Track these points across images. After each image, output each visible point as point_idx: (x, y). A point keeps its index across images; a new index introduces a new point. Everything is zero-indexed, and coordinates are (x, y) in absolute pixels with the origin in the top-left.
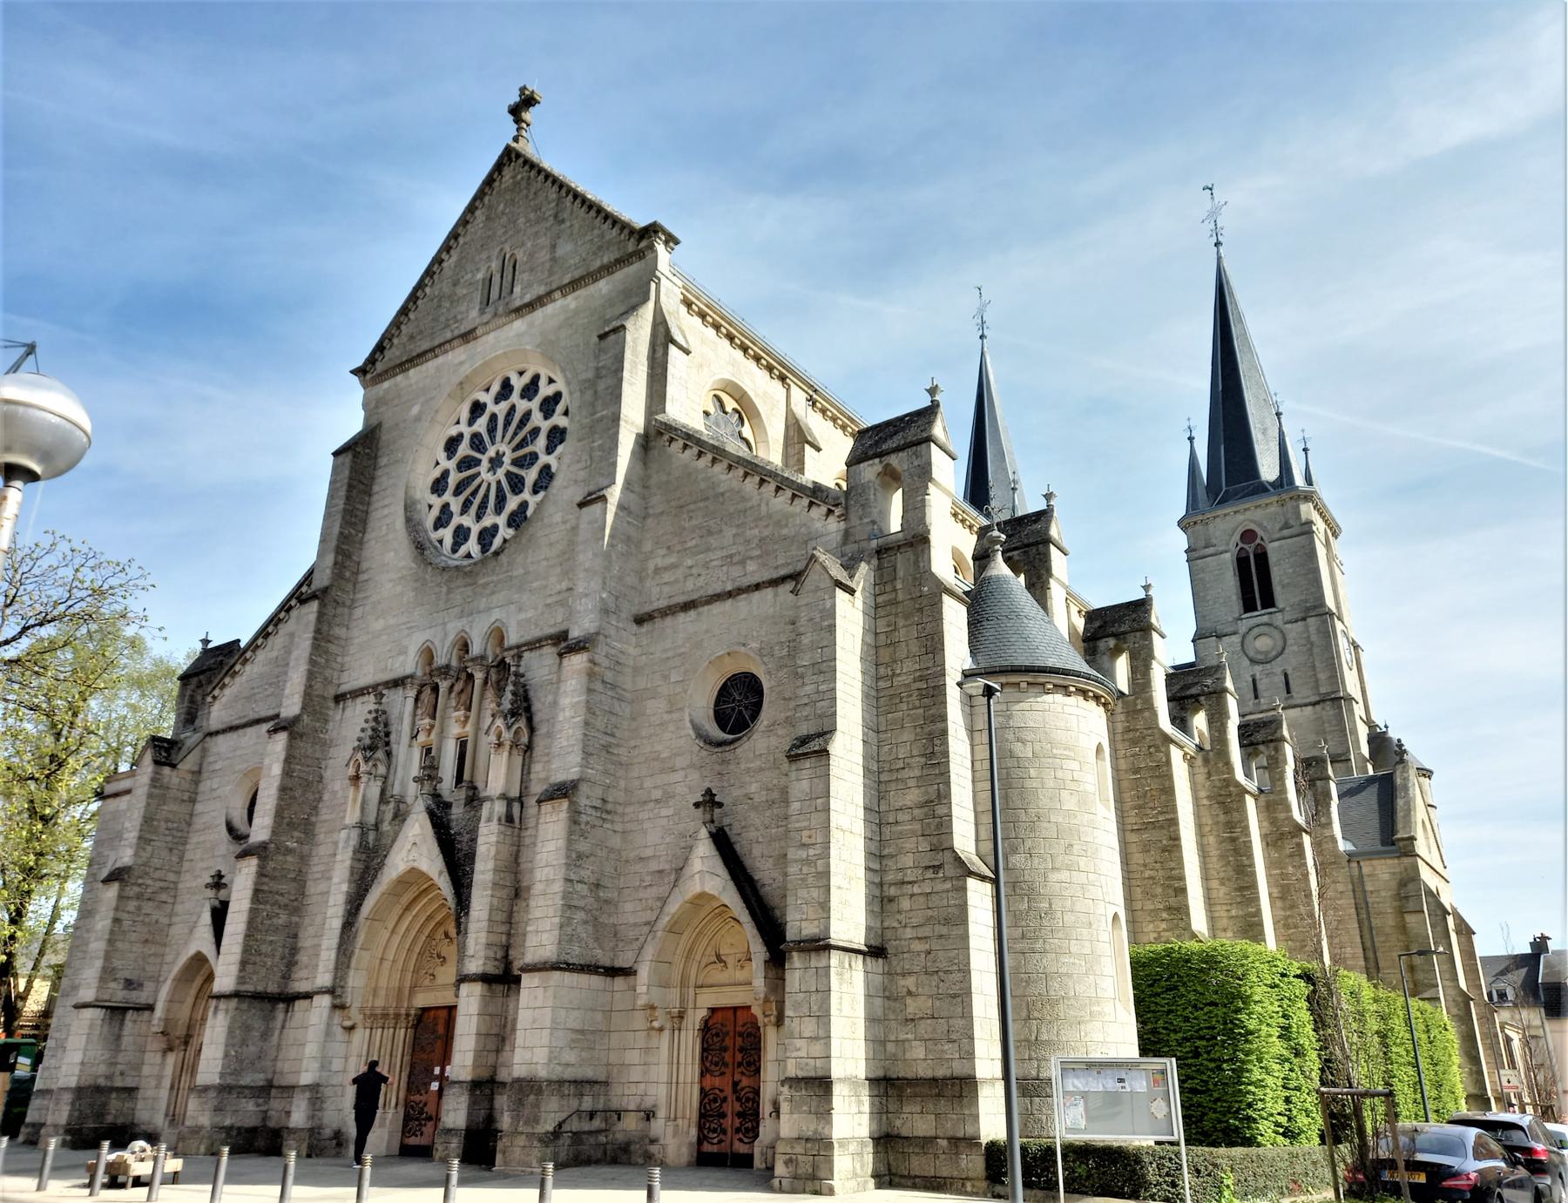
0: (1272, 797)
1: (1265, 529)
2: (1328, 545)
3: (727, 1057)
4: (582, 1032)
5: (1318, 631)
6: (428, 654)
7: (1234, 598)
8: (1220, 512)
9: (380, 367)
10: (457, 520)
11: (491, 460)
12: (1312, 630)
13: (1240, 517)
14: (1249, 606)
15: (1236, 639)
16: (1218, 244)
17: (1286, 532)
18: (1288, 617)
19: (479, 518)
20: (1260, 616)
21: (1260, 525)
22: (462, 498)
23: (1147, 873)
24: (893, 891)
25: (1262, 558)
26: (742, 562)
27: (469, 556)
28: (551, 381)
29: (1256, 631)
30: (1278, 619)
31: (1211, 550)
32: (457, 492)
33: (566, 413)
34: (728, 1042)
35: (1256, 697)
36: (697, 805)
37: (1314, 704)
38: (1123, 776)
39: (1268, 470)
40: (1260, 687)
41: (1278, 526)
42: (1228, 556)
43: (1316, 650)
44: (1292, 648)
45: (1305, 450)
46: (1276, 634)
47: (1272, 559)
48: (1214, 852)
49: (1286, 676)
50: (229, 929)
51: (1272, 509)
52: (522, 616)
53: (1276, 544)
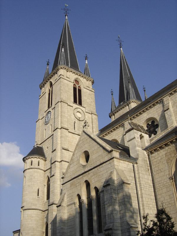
14: (75, 101)
25: (80, 91)
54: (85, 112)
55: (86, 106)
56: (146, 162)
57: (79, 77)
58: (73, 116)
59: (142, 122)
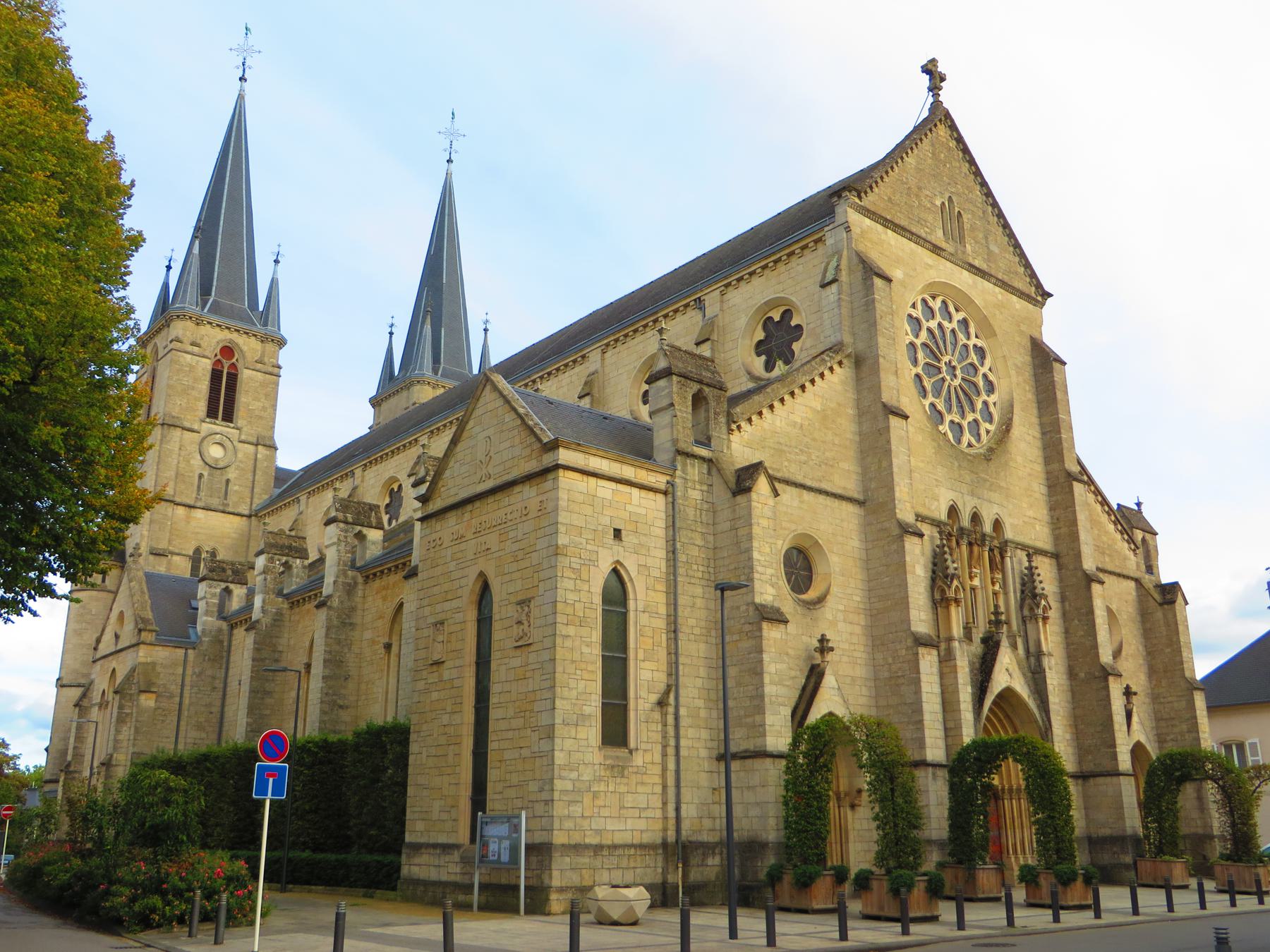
10: (938, 318)
11: (954, 368)
14: (212, 413)
16: (242, 79)
17: (259, 366)
19: (930, 330)
20: (219, 427)
22: (955, 409)
25: (233, 378)
28: (970, 445)
32: (953, 331)
33: (934, 298)
49: (485, 588)
54: (236, 443)
55: (245, 422)
56: (69, 547)
57: (234, 336)
58: (196, 461)
59: (490, 407)
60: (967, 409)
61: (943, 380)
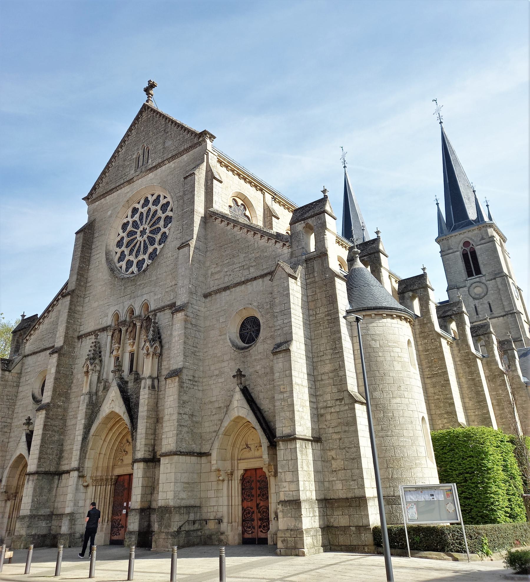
0: (489, 359)
1: (473, 241)
2: (501, 246)
3: (254, 492)
4: (188, 483)
5: (502, 284)
6: (117, 316)
7: (463, 271)
8: (453, 234)
9: (94, 196)
11: (141, 232)
12: (499, 283)
13: (462, 236)
14: (470, 274)
15: (466, 289)
17: (483, 241)
18: (487, 278)
20: (475, 278)
21: (471, 239)
22: (130, 248)
23: (436, 397)
24: (322, 411)
25: (473, 253)
26: (248, 268)
27: (133, 273)
29: (474, 285)
30: (483, 279)
31: (451, 251)
33: (172, 210)
34: (253, 485)
35: (477, 314)
36: (234, 376)
37: (503, 316)
38: (421, 353)
39: (472, 215)
40: (479, 310)
41: (479, 239)
42: (458, 253)
43: (501, 292)
44: (490, 292)
45: (487, 206)
46: (483, 286)
47: (478, 253)
48: (465, 386)
49: (489, 304)
50: (33, 443)
51: (476, 232)
52: (156, 297)
53: (479, 247)
60: (151, 213)
61: (151, 232)
